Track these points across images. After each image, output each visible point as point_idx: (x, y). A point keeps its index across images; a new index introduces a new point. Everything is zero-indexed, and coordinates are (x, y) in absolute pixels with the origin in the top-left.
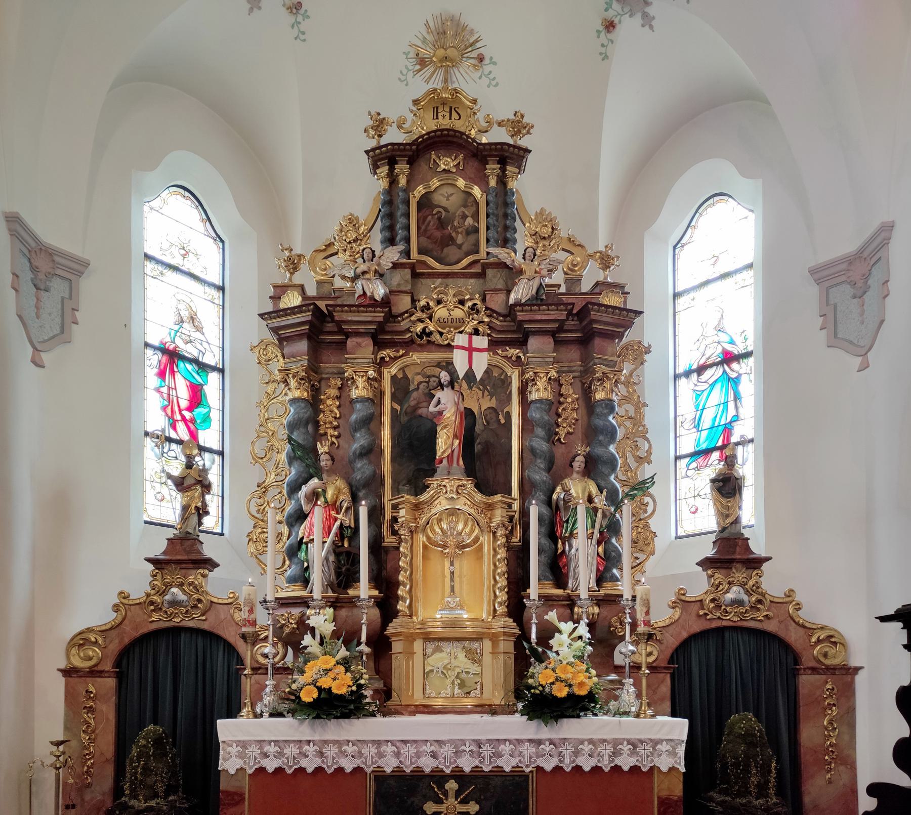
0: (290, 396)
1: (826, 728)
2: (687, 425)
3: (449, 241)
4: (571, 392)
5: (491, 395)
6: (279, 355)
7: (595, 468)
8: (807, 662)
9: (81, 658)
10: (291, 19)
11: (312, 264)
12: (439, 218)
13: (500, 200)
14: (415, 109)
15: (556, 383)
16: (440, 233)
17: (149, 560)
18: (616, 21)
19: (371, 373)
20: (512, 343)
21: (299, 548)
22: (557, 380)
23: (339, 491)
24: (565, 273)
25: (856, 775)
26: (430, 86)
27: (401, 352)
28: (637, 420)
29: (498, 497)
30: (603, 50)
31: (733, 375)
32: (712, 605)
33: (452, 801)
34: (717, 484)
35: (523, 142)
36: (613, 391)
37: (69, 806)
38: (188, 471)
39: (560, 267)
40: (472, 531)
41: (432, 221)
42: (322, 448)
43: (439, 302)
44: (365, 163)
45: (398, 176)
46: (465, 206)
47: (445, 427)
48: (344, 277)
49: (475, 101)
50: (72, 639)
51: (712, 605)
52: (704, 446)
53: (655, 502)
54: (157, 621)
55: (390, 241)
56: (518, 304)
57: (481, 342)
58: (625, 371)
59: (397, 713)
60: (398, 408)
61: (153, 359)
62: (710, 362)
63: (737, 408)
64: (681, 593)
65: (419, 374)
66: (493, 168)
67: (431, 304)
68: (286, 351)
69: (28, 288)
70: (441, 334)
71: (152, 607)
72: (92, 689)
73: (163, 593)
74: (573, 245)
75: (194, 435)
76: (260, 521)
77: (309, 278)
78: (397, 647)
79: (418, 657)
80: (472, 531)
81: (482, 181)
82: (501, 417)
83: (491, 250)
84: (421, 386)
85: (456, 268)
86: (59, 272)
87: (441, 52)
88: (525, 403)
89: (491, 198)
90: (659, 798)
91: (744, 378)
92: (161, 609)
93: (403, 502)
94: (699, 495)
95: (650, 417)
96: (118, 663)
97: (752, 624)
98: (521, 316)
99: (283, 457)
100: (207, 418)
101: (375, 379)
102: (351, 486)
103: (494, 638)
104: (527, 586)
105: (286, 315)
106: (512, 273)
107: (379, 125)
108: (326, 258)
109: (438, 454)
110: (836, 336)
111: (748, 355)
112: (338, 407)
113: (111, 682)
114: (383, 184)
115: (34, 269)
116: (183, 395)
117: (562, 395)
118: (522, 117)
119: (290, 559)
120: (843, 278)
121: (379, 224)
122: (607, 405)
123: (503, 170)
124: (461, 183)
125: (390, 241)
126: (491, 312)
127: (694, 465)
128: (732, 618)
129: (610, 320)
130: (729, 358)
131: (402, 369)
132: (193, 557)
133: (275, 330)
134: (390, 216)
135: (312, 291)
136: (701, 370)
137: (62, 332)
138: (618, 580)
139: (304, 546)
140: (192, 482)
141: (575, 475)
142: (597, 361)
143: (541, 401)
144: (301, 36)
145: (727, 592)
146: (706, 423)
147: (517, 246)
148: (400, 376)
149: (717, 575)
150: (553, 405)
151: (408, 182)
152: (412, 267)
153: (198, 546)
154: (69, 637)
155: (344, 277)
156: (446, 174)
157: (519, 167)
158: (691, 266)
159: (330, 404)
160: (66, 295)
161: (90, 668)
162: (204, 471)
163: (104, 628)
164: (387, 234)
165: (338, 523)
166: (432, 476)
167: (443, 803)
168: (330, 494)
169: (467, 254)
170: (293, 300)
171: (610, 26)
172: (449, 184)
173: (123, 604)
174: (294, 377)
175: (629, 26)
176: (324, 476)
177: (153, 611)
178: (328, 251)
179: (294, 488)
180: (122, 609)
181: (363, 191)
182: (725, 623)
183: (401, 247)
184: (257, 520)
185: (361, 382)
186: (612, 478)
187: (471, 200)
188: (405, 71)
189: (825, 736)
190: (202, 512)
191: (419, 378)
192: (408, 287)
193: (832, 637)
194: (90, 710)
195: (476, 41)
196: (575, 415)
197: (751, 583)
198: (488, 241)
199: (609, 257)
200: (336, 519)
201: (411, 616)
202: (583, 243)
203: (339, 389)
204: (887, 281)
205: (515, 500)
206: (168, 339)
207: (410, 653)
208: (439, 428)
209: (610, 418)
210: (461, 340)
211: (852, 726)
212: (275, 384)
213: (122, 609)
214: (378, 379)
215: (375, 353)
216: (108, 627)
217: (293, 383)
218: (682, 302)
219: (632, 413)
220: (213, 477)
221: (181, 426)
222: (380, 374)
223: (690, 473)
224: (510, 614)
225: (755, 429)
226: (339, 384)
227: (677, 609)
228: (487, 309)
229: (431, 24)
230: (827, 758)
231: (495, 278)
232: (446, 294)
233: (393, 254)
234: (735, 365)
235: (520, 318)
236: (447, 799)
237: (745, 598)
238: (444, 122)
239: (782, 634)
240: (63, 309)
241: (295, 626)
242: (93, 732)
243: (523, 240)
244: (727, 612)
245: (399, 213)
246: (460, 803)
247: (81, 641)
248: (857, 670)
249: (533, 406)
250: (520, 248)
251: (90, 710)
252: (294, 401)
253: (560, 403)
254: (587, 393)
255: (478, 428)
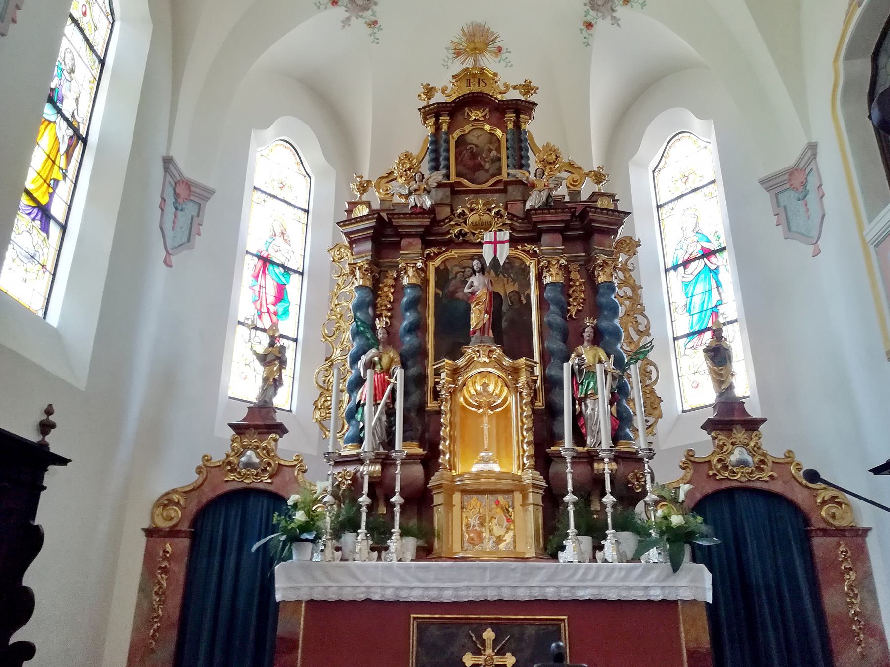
0: (357, 284)
1: (848, 595)
2: (680, 311)
3: (479, 167)
4: (578, 277)
5: (514, 281)
6: (349, 254)
7: (602, 338)
8: (817, 524)
9: (164, 518)
10: (370, 30)
11: (378, 187)
12: (472, 152)
13: (516, 146)
14: (454, 81)
15: (566, 269)
16: (472, 161)
17: (231, 425)
18: (593, 22)
19: (420, 264)
20: (531, 240)
21: (357, 411)
22: (566, 267)
23: (392, 360)
24: (568, 187)
25: (887, 647)
26: (464, 66)
27: (443, 249)
28: (635, 299)
29: (522, 360)
30: (586, 40)
31: (713, 267)
32: (719, 466)
33: (489, 651)
34: (709, 354)
35: (531, 99)
36: (612, 275)
37: (138, 657)
38: (271, 349)
39: (564, 183)
40: (501, 392)
41: (466, 154)
42: (379, 324)
43: (472, 210)
44: (419, 116)
45: (441, 124)
46: (491, 143)
47: (477, 304)
48: (401, 195)
49: (495, 74)
50: (159, 500)
51: (719, 466)
52: (696, 328)
53: (657, 369)
54: (233, 482)
55: (435, 168)
56: (533, 209)
57: (505, 235)
58: (620, 260)
59: (439, 558)
60: (440, 293)
61: (250, 264)
62: (693, 256)
63: (720, 294)
64: (690, 454)
65: (456, 266)
66: (510, 116)
67: (466, 211)
68: (355, 250)
69: (170, 209)
70: (474, 234)
71: (229, 468)
72: (168, 548)
73: (240, 454)
74: (572, 167)
75: (275, 326)
76: (325, 389)
77: (375, 197)
78: (438, 499)
79: (457, 510)
80: (501, 392)
81: (503, 127)
82: (522, 298)
83: (510, 171)
84: (458, 275)
85: (485, 186)
86: (192, 198)
87: (472, 46)
88: (541, 287)
89: (509, 137)
90: (687, 650)
91: (722, 269)
92: (236, 470)
93: (443, 367)
94: (698, 372)
95: (647, 297)
96: (194, 523)
97: (759, 485)
98: (535, 218)
99: (348, 335)
100: (286, 312)
101: (422, 270)
102: (401, 355)
103: (523, 491)
104: (557, 438)
105: (357, 222)
106: (527, 187)
107: (429, 91)
108: (388, 182)
109: (473, 323)
110: (789, 229)
111: (723, 249)
112: (392, 294)
113: (184, 543)
114: (430, 130)
115: (176, 195)
116: (271, 292)
117: (571, 280)
118: (530, 82)
119: (349, 422)
120: (787, 186)
121: (427, 157)
122: (608, 286)
123: (518, 117)
124: (487, 127)
125: (435, 168)
126: (512, 216)
127: (690, 345)
128: (739, 478)
129: (605, 220)
130: (707, 254)
131: (444, 262)
132: (268, 423)
133: (347, 234)
134: (436, 151)
135: (376, 206)
136: (686, 264)
137: (189, 240)
138: (631, 439)
139: (360, 409)
140: (273, 359)
141: (586, 344)
142: (597, 251)
143: (553, 284)
144: (376, 41)
145: (731, 453)
146: (696, 308)
147: (530, 170)
148: (442, 268)
149: (720, 437)
150: (565, 288)
151: (449, 128)
152: (452, 186)
153: (273, 413)
154: (155, 499)
155: (401, 195)
156: (477, 126)
157: (530, 115)
158: (668, 185)
159: (387, 291)
160: (195, 214)
161: (171, 527)
162: (283, 348)
163: (187, 489)
164: (433, 164)
165: (389, 387)
166: (468, 344)
167: (481, 654)
168: (385, 360)
169: (493, 176)
170: (363, 211)
171: (589, 25)
172: (478, 127)
173: (206, 468)
174: (360, 269)
175: (602, 25)
176: (381, 347)
177: (229, 471)
178: (389, 177)
179: (355, 359)
180: (204, 471)
181: (416, 135)
182: (734, 484)
183: (444, 172)
184: (322, 390)
185: (411, 272)
186: (619, 346)
187: (494, 138)
188: (446, 59)
189: (849, 604)
190: (277, 383)
191: (457, 269)
192: (448, 201)
193: (836, 497)
194: (164, 570)
195: (496, 38)
196: (583, 296)
197: (752, 444)
198: (508, 166)
199: (601, 174)
200: (389, 383)
201: (451, 470)
202: (580, 165)
203: (395, 279)
204: (821, 186)
205: (537, 363)
206: (264, 249)
207: (449, 505)
208: (472, 306)
209: (613, 297)
210: (488, 236)
211: (873, 593)
212: (345, 277)
213: (204, 471)
214: (424, 270)
215: (423, 249)
216: (192, 487)
217: (358, 274)
218: (663, 211)
219: (630, 293)
220: (289, 355)
221: (266, 317)
222: (426, 266)
223: (687, 352)
224: (536, 468)
225: (738, 310)
226: (395, 275)
227: (688, 470)
228: (509, 214)
229: (466, 30)
230: (854, 628)
231: (514, 192)
232: (477, 203)
233: (438, 176)
234: (713, 259)
235: (534, 220)
236: (484, 650)
237: (749, 459)
238: (475, 88)
239: (789, 495)
240: (191, 224)
241: (349, 482)
242: (164, 593)
243: (534, 163)
244: (734, 473)
245: (441, 150)
246: (497, 654)
247: (165, 501)
248: (866, 531)
249: (548, 288)
250: (532, 170)
251: (164, 570)
252: (359, 288)
253: (571, 286)
254: (591, 278)
255: (504, 308)
